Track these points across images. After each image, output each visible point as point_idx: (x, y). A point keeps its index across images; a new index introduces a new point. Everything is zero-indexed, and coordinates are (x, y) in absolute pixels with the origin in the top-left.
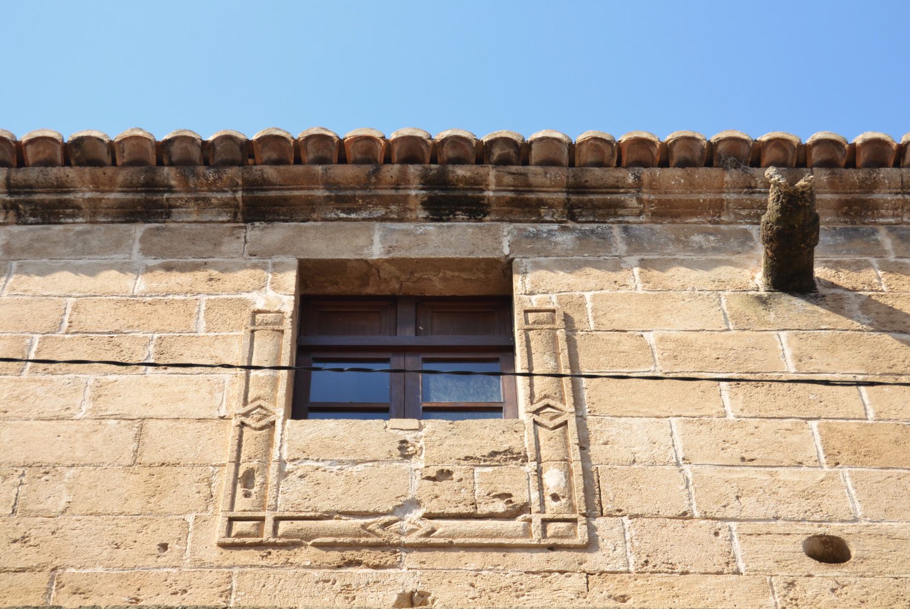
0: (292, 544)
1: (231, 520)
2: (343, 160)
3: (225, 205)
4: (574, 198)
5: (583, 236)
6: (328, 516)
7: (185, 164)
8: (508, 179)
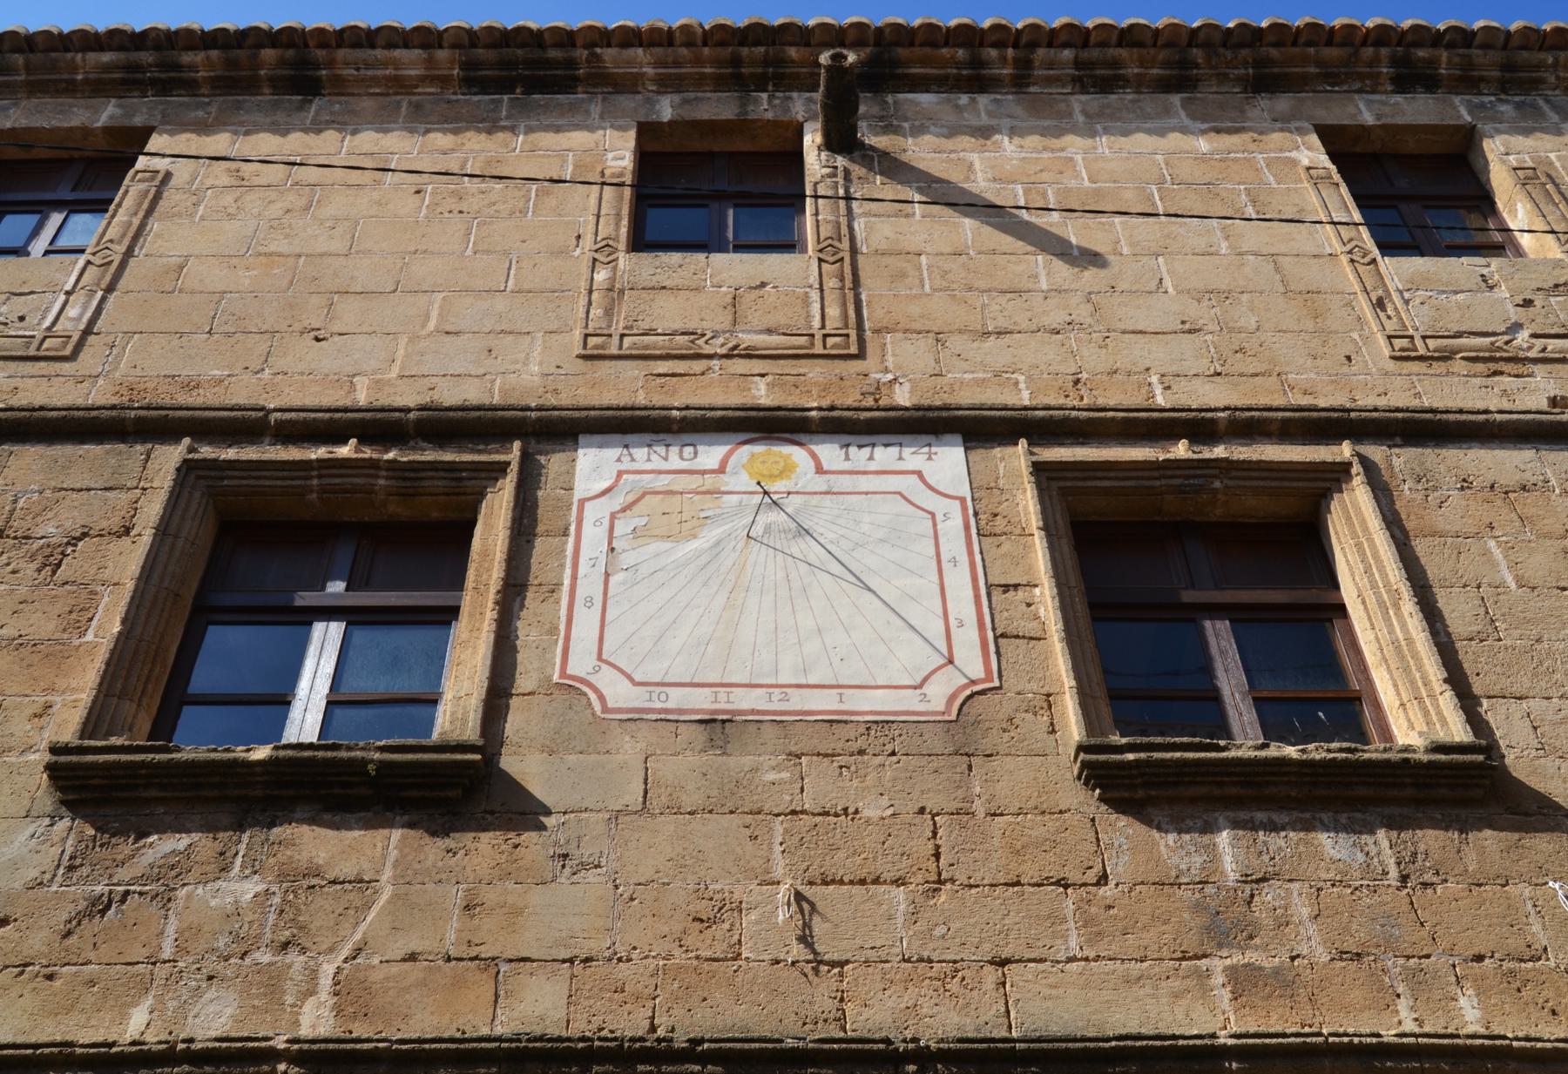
0: (1446, 356)
1: (587, 336)
2: (1329, 43)
3: (1239, 79)
4: (1508, 75)
5: (1519, 106)
6: (1458, 335)
7: (1207, 45)
8: (1456, 60)
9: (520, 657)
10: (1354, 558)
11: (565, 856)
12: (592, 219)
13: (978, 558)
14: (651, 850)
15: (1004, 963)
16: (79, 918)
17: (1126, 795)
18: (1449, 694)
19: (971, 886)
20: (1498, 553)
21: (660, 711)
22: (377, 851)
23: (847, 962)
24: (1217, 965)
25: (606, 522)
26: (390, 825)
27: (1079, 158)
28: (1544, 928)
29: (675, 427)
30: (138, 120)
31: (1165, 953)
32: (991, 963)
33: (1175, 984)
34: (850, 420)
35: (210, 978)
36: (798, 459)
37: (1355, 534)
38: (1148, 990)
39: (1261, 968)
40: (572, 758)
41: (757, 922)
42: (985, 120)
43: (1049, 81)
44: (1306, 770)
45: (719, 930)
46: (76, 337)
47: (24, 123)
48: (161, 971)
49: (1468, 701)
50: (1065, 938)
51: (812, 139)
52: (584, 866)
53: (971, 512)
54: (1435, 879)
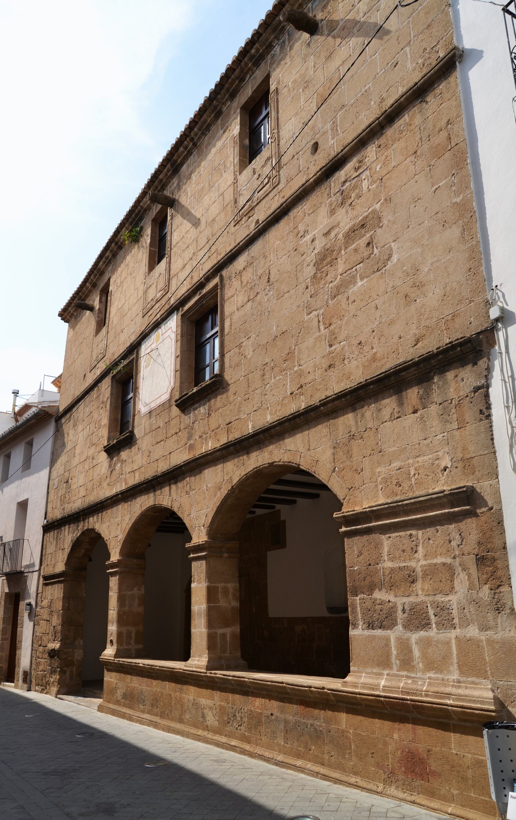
30: (259, 80)
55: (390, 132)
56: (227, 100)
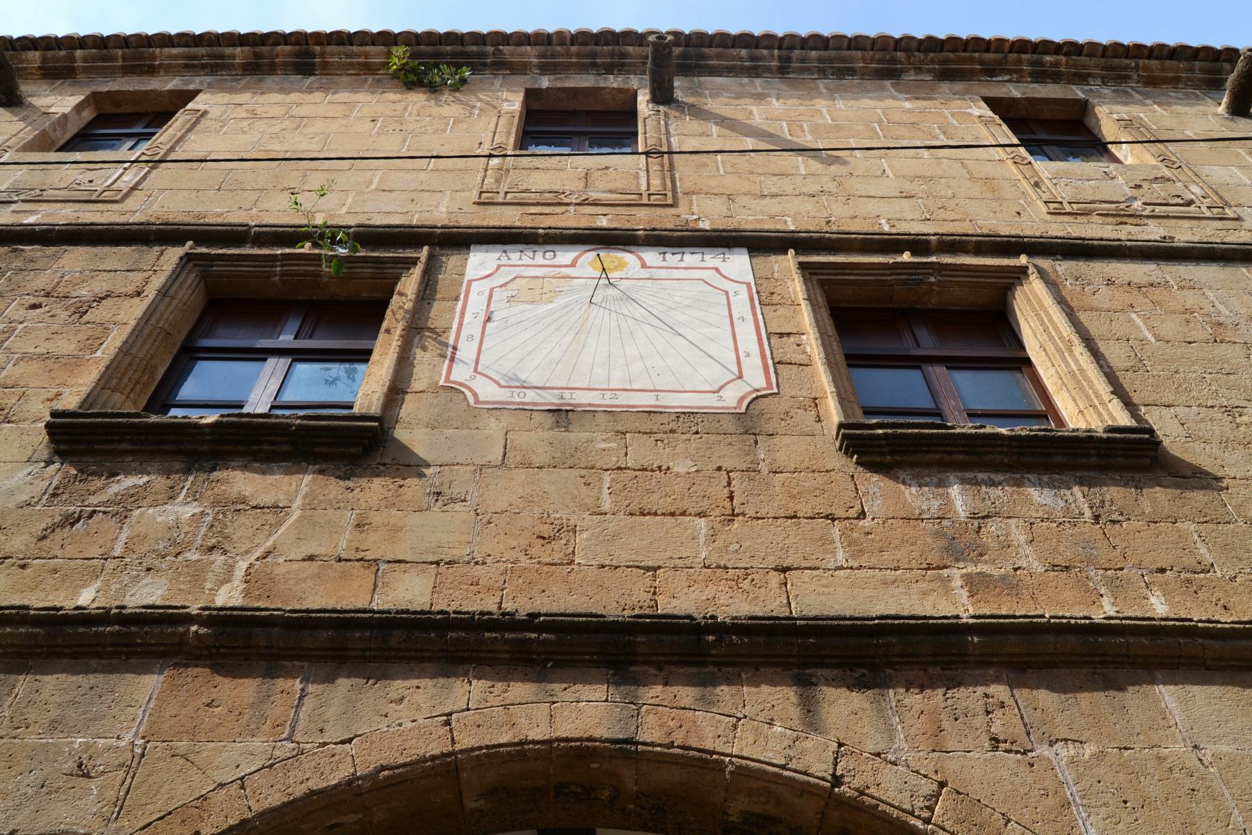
2: (988, 51)
9: (415, 370)
10: (1035, 323)
11: (439, 494)
12: (491, 135)
13: (760, 317)
14: (505, 492)
15: (785, 570)
16: (54, 528)
17: (878, 459)
18: (1116, 401)
19: (758, 518)
20: (1139, 321)
21: (519, 404)
22: (294, 488)
23: (659, 567)
24: (955, 575)
25: (487, 293)
26: (305, 472)
27: (824, 110)
28: (1209, 550)
29: (541, 240)
30: (192, 87)
31: (914, 564)
32: (775, 570)
33: (924, 586)
34: (666, 236)
35: (149, 569)
36: (628, 259)
37: (1036, 316)
38: (902, 589)
39: (990, 576)
40: (449, 432)
41: (587, 540)
42: (760, 90)
43: (802, 70)
44: (1014, 443)
45: (558, 545)
46: (125, 191)
47: (117, 88)
48: (110, 564)
49: (1129, 405)
50: (834, 553)
51: (643, 98)
52: (453, 501)
53: (754, 291)
54: (1120, 518)
55: (865, 615)
56: (929, 71)
